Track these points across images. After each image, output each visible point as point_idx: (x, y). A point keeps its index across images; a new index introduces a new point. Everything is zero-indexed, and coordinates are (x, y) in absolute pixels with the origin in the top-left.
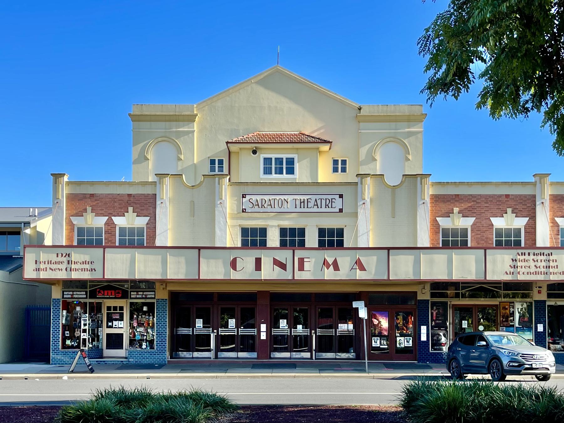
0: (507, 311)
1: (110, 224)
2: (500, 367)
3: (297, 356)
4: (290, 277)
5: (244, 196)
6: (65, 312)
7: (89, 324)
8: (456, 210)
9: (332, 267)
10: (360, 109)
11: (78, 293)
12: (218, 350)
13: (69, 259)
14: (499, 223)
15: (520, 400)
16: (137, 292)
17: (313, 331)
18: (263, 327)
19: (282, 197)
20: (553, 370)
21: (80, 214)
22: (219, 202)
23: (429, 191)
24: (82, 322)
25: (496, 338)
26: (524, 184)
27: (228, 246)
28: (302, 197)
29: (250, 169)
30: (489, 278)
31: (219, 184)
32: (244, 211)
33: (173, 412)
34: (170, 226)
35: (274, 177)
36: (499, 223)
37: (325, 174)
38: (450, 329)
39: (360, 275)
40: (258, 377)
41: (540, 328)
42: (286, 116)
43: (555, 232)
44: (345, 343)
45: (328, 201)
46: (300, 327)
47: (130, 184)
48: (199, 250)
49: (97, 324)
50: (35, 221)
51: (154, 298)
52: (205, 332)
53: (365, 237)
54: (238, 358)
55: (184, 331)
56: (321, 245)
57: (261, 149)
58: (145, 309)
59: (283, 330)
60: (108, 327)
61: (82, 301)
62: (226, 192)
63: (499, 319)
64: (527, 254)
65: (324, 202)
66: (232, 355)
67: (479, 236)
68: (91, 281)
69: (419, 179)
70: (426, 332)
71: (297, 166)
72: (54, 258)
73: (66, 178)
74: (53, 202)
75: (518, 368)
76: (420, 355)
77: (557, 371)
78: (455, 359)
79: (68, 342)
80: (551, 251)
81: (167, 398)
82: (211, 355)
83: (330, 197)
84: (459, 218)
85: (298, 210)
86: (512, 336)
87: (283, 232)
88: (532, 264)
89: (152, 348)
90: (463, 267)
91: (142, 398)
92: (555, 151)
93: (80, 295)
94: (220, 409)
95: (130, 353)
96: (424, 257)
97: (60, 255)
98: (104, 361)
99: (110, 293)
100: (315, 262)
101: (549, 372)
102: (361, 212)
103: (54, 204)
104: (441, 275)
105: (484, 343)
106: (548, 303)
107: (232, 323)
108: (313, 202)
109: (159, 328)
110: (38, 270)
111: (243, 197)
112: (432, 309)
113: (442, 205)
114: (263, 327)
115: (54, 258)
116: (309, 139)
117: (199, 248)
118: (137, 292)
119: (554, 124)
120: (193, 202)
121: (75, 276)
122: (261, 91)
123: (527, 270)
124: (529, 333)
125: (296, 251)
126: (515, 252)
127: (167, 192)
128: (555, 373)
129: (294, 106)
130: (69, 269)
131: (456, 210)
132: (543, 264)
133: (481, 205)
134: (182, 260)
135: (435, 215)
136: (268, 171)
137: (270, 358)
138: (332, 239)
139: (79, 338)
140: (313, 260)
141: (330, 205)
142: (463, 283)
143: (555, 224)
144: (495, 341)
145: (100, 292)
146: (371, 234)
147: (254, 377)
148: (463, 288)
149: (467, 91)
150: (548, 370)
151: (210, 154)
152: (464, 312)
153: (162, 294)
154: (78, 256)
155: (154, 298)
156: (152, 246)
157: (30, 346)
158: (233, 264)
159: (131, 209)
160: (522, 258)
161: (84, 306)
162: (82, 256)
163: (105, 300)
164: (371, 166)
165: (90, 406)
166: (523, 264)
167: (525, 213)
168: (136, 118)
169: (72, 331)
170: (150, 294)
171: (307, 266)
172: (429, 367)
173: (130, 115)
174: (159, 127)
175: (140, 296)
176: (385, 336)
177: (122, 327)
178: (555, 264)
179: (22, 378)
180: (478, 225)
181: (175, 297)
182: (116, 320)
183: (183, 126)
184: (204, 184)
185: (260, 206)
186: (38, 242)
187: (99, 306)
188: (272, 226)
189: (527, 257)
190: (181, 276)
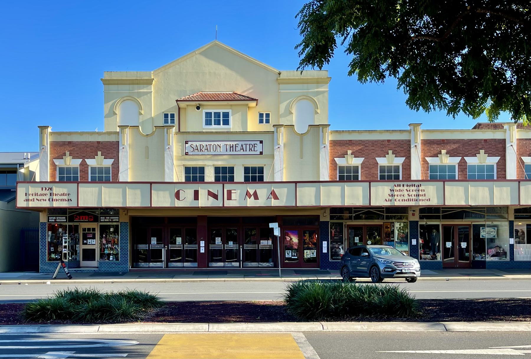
0: (389, 230)
1: (84, 165)
2: (378, 272)
3: (229, 265)
4: (221, 205)
5: (186, 143)
6: (50, 233)
7: (69, 242)
8: (349, 152)
9: (252, 197)
10: (280, 74)
11: (60, 218)
12: (168, 261)
13: (51, 192)
14: (382, 162)
15: (369, 297)
17: (241, 246)
18: (202, 244)
19: (216, 143)
20: (418, 274)
21: (60, 157)
22: (167, 147)
23: (329, 137)
24: (63, 240)
25: (376, 250)
26: (401, 131)
27: (174, 181)
28: (232, 143)
29: (195, 121)
30: (373, 204)
31: (167, 133)
32: (187, 154)
33: (111, 307)
34: (129, 166)
35: (214, 128)
36: (382, 162)
37: (253, 125)
38: (346, 244)
39: (274, 203)
40: (197, 281)
41: (414, 242)
42: (223, 79)
43: (426, 169)
44: (267, 255)
45: (251, 146)
46: (231, 243)
47: (99, 134)
48: (151, 184)
49: (75, 241)
50: (28, 162)
51: (118, 222)
52: (158, 247)
53: (279, 173)
54: (183, 267)
55: (142, 247)
56: (247, 180)
57: (203, 105)
58: (112, 230)
59: (219, 246)
60: (84, 244)
61: (64, 224)
62: (172, 140)
63: (384, 237)
64: (402, 185)
65: (248, 146)
66: (179, 264)
67: (367, 172)
68: (70, 209)
69: (321, 128)
70: (326, 246)
71: (231, 119)
72: (39, 191)
73: (49, 130)
74: (40, 147)
75: (392, 273)
76: (321, 264)
77: (422, 275)
78: (346, 266)
79: (53, 256)
80: (420, 183)
81: (108, 297)
82: (162, 265)
83: (253, 143)
84: (447, 157)
85: (229, 153)
86: (389, 249)
87: (217, 170)
88: (406, 193)
89: (117, 259)
90: (353, 196)
91: (95, 296)
92: (408, 106)
93: (62, 219)
94: (149, 304)
95: (100, 263)
96: (323, 189)
97: (44, 189)
98: (81, 270)
99: (84, 218)
100: (240, 194)
101: (415, 275)
102: (276, 153)
103: (41, 150)
104: (336, 202)
105: (367, 254)
106: (420, 223)
107: (179, 240)
108: (240, 147)
109: (123, 244)
110: (27, 200)
111: (186, 143)
112: (331, 228)
113: (339, 148)
114: (202, 244)
115: (39, 191)
116: (241, 97)
117: (151, 183)
119: (407, 86)
120: (147, 148)
121: (56, 204)
122: (204, 61)
123: (402, 198)
124: (405, 246)
125: (225, 185)
126: (392, 184)
127: (127, 140)
128: (420, 277)
129: (229, 71)
130: (51, 200)
131: (349, 152)
132: (414, 193)
133: (369, 149)
134: (138, 192)
135: (425, 154)
136: (208, 123)
137: (208, 267)
138: (254, 175)
139: (61, 252)
140: (239, 191)
141: (253, 149)
142: (355, 208)
143: (425, 162)
144: (375, 253)
145: (77, 217)
146: (284, 171)
147: (194, 281)
148: (355, 212)
149: (328, 63)
150: (415, 274)
152: (357, 230)
153: (125, 219)
154: (58, 189)
155: (118, 222)
156: (116, 181)
157: (24, 259)
158: (177, 195)
159: (99, 153)
160: (398, 188)
161: (64, 228)
162: (61, 189)
163: (81, 223)
164: (288, 118)
165: (47, 302)
166: (399, 193)
167: (403, 154)
168: (107, 82)
169: (56, 247)
170: (116, 219)
171: (233, 196)
172: (328, 273)
173: (102, 80)
174: (125, 89)
175: (108, 220)
176: (295, 249)
177: (94, 244)
178: (423, 193)
179: (16, 283)
180: (367, 163)
182: (90, 238)
183: (143, 88)
184: (156, 133)
185: (199, 150)
186: (30, 179)
187: (77, 227)
188: (208, 166)
189: (401, 188)
190: (137, 204)
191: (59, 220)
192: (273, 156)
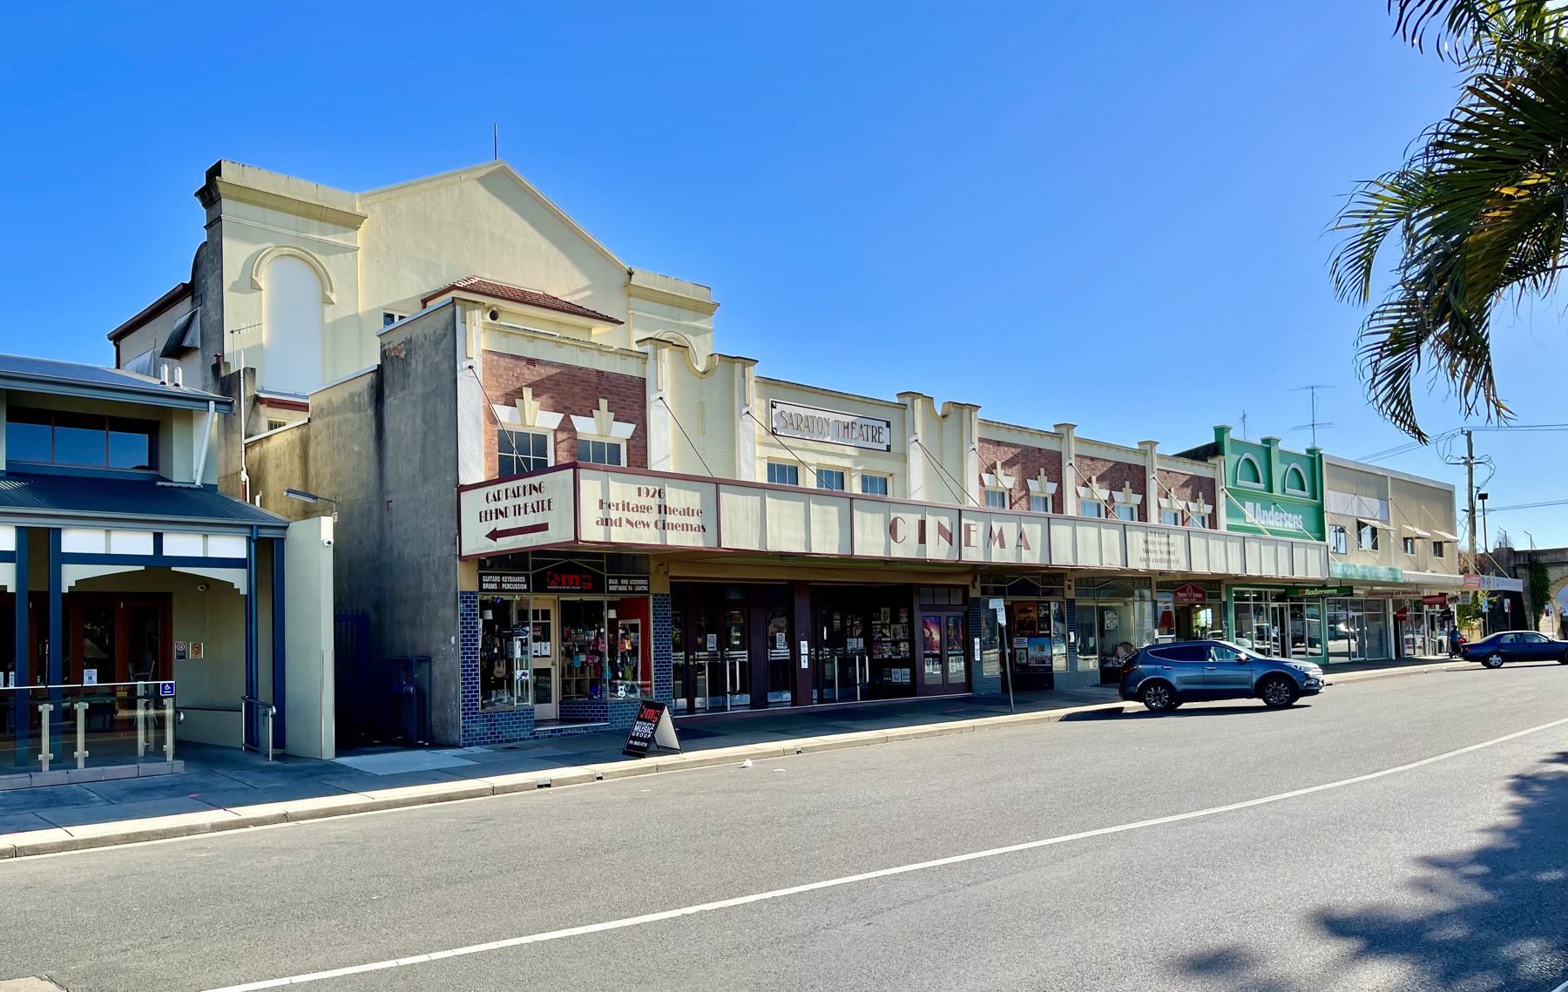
1: (566, 426)
10: (631, 274)
11: (511, 579)
16: (620, 579)
83: (877, 424)
93: (514, 582)
118: (620, 579)
120: (701, 405)
122: (480, 194)
127: (664, 379)
151: (387, 301)
153: (660, 586)
181: (681, 591)
183: (335, 233)
191: (508, 586)
192: (904, 457)
